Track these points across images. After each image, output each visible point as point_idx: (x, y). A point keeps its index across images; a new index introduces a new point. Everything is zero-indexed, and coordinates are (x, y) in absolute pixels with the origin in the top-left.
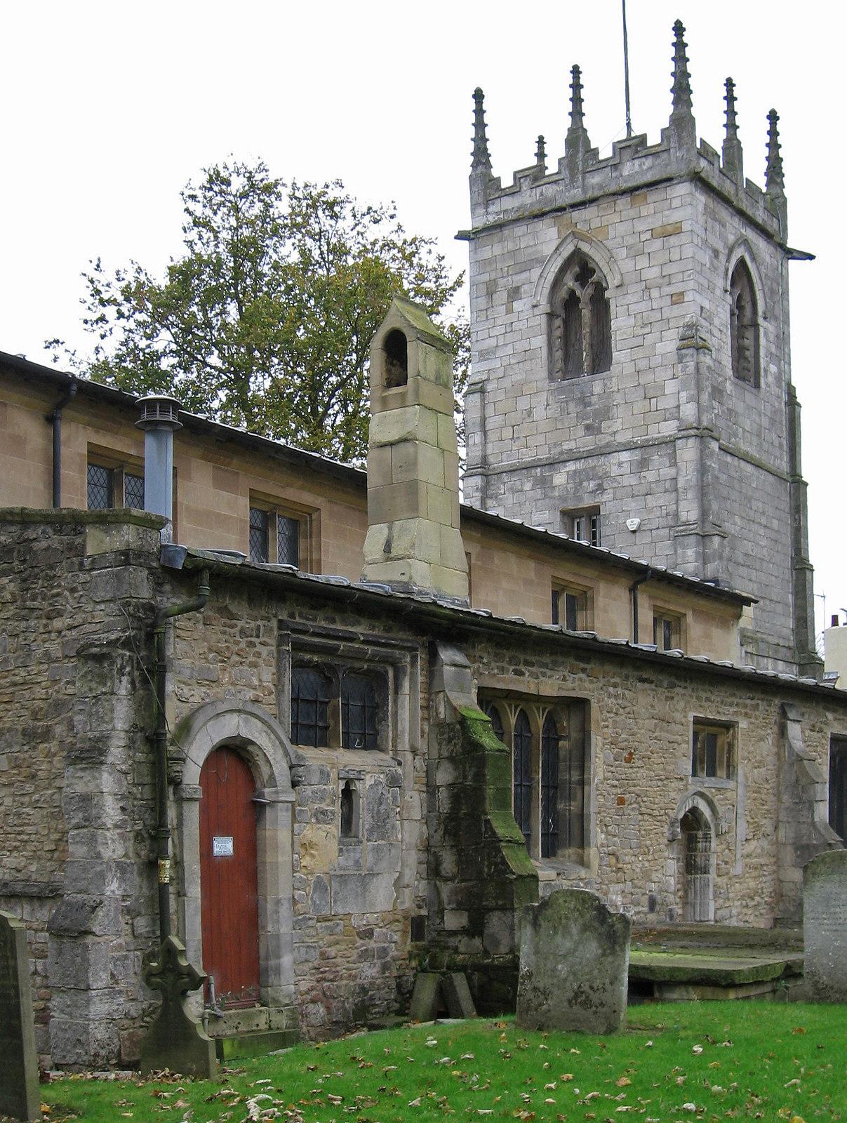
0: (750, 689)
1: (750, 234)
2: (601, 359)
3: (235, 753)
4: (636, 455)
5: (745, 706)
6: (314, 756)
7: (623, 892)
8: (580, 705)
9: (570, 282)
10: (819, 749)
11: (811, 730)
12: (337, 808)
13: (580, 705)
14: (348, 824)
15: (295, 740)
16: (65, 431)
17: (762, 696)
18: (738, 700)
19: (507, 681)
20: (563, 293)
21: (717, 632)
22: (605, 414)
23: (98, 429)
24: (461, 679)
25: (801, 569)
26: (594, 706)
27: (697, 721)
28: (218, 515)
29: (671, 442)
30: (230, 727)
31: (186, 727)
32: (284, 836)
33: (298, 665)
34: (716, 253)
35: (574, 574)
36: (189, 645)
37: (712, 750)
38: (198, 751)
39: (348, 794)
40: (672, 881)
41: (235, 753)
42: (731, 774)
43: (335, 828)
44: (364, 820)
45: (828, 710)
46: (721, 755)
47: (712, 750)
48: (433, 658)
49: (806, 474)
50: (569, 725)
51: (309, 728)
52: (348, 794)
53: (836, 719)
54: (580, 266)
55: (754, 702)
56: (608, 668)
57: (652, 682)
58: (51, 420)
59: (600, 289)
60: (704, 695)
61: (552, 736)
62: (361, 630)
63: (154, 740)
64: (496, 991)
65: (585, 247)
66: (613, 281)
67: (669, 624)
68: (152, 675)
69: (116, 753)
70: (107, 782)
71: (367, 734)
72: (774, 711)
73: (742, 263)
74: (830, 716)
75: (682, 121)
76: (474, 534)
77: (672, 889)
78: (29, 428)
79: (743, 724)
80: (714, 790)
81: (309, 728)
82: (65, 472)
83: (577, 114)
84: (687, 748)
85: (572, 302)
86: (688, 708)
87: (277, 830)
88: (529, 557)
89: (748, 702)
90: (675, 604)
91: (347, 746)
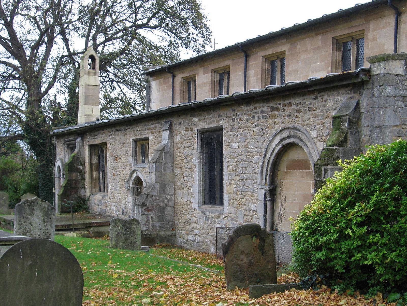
0: (151, 120)
4: (8, 87)
5: (151, 129)
7: (115, 206)
10: (192, 140)
11: (186, 131)
17: (157, 121)
18: (147, 127)
23: (182, 73)
28: (204, 83)
35: (349, 28)
40: (130, 205)
45: (194, 116)
53: (200, 120)
55: (154, 126)
56: (108, 130)
57: (120, 130)
60: (135, 129)
74: (196, 119)
76: (283, 41)
77: (130, 208)
79: (150, 138)
80: (141, 169)
84: (131, 153)
88: (317, 35)
89: (152, 126)
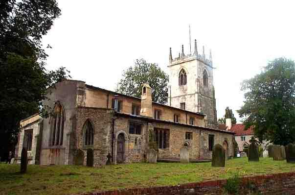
1: (205, 66)
2: (185, 83)
3: (122, 135)
6: (131, 135)
8: (168, 130)
9: (182, 73)
12: (134, 141)
13: (168, 130)
14: (136, 143)
15: (130, 133)
16: (109, 97)
19: (158, 127)
20: (181, 74)
21: (200, 120)
22: (186, 90)
24: (151, 127)
25: (215, 111)
26: (170, 130)
27: (186, 132)
29: (194, 94)
30: (120, 132)
31: (116, 132)
32: (127, 144)
33: (131, 125)
34: (201, 69)
36: (118, 122)
37: (189, 136)
38: (117, 135)
39: (136, 140)
41: (122, 135)
42: (192, 139)
43: (134, 143)
44: (138, 143)
46: (191, 137)
47: (189, 136)
48: (147, 124)
49: (216, 97)
50: (167, 132)
51: (131, 131)
52: (136, 140)
54: (183, 70)
58: (108, 96)
59: (185, 73)
61: (165, 133)
62: (138, 121)
63: (112, 133)
64: (145, 162)
65: (184, 68)
66: (187, 73)
67: (192, 119)
68: (113, 125)
69: (108, 134)
70: (107, 137)
71: (139, 132)
72: (199, 131)
73: (205, 70)
75: (196, 52)
78: (105, 97)
81: (131, 131)
82: (194, 45)
83: (183, 51)
85: (182, 75)
86: (184, 131)
87: (127, 144)
90: (193, 116)
91: (137, 134)
